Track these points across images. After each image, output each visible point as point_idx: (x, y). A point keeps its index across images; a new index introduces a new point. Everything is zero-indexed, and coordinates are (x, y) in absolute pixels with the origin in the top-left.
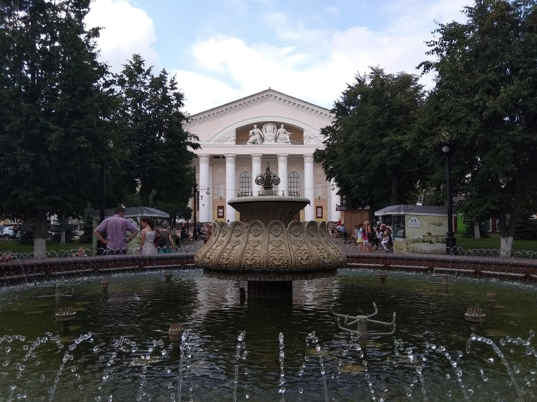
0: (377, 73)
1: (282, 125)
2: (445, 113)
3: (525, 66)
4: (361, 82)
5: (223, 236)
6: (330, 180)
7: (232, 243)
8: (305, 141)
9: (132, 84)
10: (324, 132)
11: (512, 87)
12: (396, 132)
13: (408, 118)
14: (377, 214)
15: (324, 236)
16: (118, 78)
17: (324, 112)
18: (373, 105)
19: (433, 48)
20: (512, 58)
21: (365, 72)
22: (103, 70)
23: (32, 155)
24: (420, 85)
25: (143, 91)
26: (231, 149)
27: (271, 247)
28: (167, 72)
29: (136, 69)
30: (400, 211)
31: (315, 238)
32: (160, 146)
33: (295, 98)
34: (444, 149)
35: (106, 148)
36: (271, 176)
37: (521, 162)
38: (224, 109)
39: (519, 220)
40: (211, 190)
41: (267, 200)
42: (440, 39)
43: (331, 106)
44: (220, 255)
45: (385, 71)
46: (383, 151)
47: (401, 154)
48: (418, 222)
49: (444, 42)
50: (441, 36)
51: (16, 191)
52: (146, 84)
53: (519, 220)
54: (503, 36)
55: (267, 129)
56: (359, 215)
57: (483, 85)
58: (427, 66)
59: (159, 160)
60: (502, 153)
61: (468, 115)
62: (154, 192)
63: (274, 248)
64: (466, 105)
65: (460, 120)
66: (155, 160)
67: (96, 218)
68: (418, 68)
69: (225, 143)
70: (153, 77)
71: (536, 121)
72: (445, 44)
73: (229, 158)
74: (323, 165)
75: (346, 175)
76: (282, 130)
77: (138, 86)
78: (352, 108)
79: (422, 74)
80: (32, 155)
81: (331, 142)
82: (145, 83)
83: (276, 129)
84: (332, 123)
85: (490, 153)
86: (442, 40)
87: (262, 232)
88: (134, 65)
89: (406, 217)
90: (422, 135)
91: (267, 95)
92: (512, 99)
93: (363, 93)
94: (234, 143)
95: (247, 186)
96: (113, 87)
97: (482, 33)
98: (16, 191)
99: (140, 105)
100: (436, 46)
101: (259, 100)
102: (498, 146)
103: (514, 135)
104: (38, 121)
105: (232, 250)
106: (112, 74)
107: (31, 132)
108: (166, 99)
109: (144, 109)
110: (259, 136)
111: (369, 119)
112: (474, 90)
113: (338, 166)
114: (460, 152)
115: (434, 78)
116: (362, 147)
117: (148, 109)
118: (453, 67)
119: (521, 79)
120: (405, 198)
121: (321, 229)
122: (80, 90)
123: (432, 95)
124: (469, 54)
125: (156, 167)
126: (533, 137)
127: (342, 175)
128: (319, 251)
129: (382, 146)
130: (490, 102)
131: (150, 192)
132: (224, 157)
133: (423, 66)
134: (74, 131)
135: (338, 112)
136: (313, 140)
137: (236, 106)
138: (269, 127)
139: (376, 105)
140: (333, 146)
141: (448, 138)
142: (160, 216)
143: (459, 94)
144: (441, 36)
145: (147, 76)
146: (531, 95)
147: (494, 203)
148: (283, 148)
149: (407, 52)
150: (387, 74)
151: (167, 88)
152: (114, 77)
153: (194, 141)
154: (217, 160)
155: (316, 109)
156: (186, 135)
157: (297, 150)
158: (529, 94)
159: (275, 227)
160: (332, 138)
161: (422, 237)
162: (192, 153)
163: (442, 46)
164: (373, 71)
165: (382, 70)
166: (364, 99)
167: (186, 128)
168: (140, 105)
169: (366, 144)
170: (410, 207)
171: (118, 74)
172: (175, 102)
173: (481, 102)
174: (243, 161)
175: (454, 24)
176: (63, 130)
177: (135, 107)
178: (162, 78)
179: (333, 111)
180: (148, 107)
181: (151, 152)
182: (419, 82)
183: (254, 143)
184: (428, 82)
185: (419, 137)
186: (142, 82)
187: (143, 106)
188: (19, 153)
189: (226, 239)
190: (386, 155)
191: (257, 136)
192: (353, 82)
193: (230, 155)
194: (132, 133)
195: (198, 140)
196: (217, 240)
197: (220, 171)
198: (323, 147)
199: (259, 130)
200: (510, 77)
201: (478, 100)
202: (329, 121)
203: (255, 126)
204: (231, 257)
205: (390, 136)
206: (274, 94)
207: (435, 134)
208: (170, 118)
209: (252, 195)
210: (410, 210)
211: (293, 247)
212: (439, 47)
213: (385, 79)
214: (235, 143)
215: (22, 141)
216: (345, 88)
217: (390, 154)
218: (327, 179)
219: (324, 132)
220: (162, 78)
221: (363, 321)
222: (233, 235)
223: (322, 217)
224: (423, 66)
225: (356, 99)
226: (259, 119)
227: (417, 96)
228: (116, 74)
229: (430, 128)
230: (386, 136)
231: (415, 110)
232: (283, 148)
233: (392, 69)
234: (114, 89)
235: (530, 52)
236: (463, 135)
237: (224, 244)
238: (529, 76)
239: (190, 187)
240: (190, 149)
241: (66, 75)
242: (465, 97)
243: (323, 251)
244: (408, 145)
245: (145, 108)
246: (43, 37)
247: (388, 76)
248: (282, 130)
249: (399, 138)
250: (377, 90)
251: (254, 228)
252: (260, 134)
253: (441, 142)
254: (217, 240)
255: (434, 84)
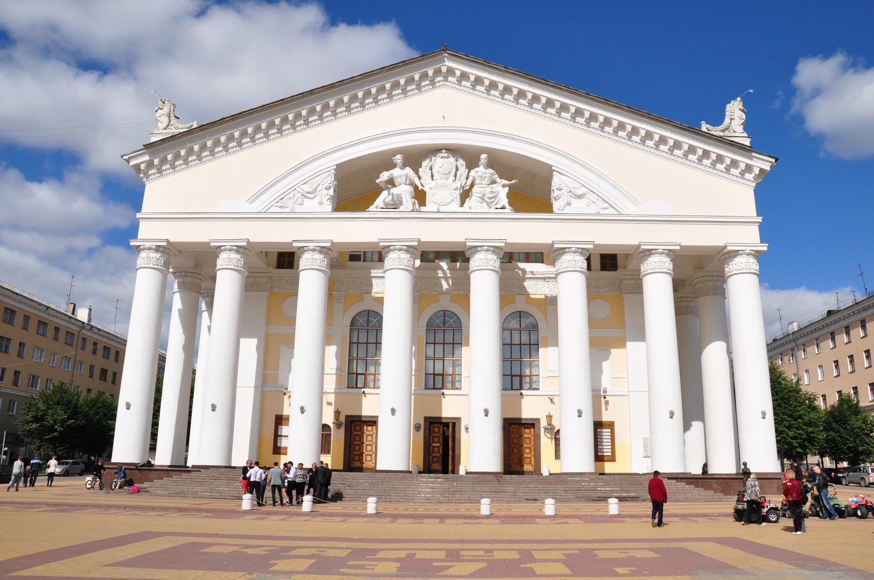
1: (484, 156)
8: (556, 206)
26: (320, 228)
76: (481, 172)
83: (463, 170)
94: (328, 207)
95: (516, 349)
110: (410, 189)
138: (442, 163)
148: (489, 223)
157: (529, 231)
174: (353, 264)
191: (404, 191)
199: (408, 170)
223: (612, 459)
232: (489, 223)
248: (481, 172)
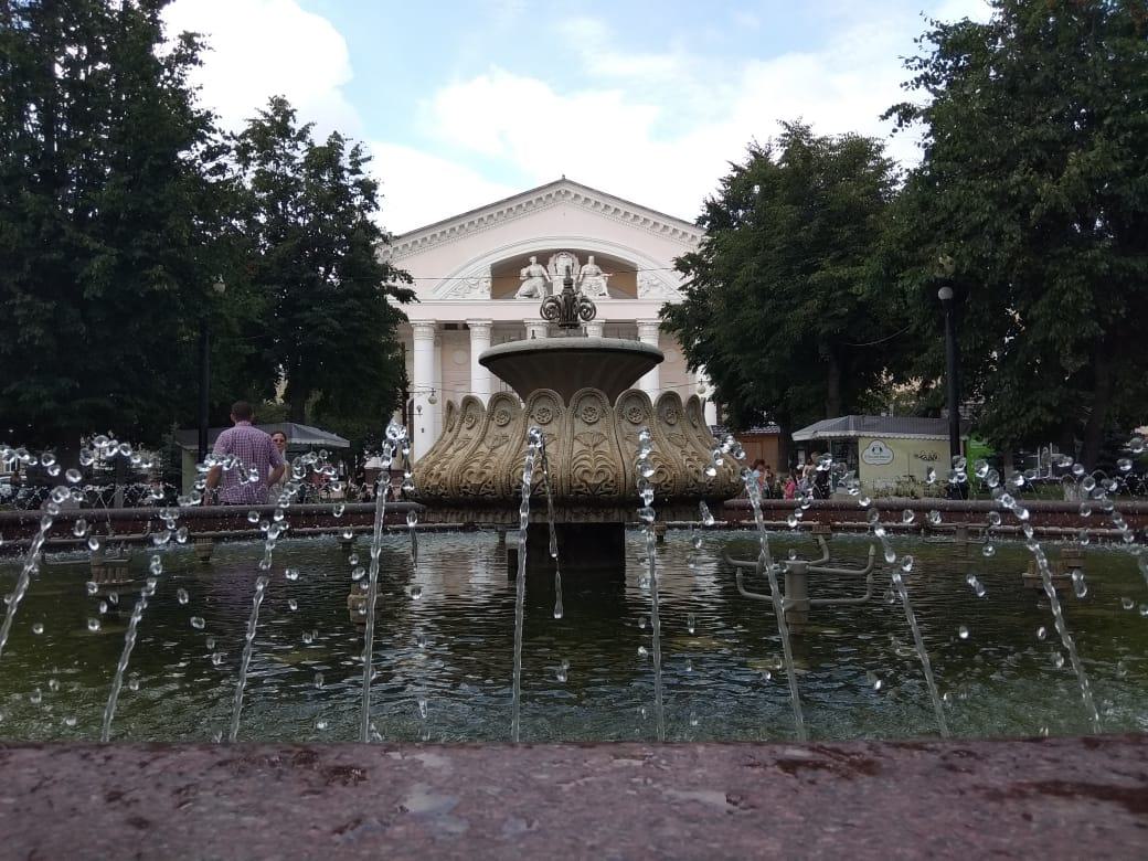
0: (796, 138)
1: (591, 258)
2: (945, 215)
3: (1117, 108)
4: (760, 158)
5: (469, 429)
6: (695, 371)
7: (489, 442)
8: (640, 292)
9: (264, 161)
10: (682, 265)
11: (1091, 155)
12: (836, 262)
13: (863, 231)
14: (798, 436)
15: (695, 427)
16: (234, 141)
17: (682, 228)
18: (786, 204)
19: (920, 73)
20: (1089, 92)
21: (769, 136)
22: (200, 125)
23: (49, 306)
24: (889, 159)
25: (290, 175)
26: (480, 308)
27: (578, 447)
28: (343, 137)
29: (273, 130)
30: (847, 429)
31: (678, 430)
32: (330, 295)
33: (619, 199)
34: (943, 293)
35: (210, 294)
36: (575, 299)
37: (1110, 318)
38: (465, 222)
39: (1101, 451)
40: (438, 395)
41: (569, 346)
42: (934, 53)
43: (693, 210)
44: (464, 467)
45: (812, 131)
46: (809, 303)
47: (849, 308)
48: (886, 452)
49: (942, 61)
50: (937, 47)
51: (13, 387)
52: (296, 161)
53: (1101, 451)
54: (1069, 46)
55: (559, 266)
56: (758, 445)
57: (1026, 151)
58: (906, 113)
59: (327, 324)
60: (1069, 297)
61: (994, 216)
62: (316, 396)
63: (585, 448)
64: (991, 195)
65: (977, 230)
66: (317, 325)
67: (188, 448)
68: (884, 118)
69: (468, 297)
70: (311, 144)
71: (1139, 231)
72: (943, 67)
73: (477, 329)
74: (680, 335)
75: (730, 356)
76: (590, 267)
77: (278, 165)
78: (741, 212)
79: (895, 131)
80: (49, 306)
81: (696, 288)
82: (294, 158)
84: (700, 246)
85: (1044, 300)
86: (938, 58)
87: (558, 414)
88: (271, 119)
89: (861, 442)
90: (895, 264)
91: (559, 191)
92: (1090, 180)
93: (765, 180)
96: (222, 159)
97: (1025, 41)
98: (13, 387)
99: (285, 207)
100: (925, 70)
101: (540, 204)
102: (1061, 282)
103: (1095, 259)
104: (61, 232)
105: (490, 455)
106: (223, 133)
107: (47, 257)
108: (341, 193)
109: (291, 214)
110: (541, 280)
111: (779, 233)
112: (1006, 164)
113: (712, 338)
114: (973, 300)
115: (920, 139)
116: (763, 293)
117: (300, 214)
118: (964, 113)
119: (1110, 137)
120: (856, 398)
121: (690, 412)
122: (151, 165)
123: (915, 177)
124: (998, 85)
125: (320, 340)
126: (1133, 264)
127: (720, 356)
128: (685, 458)
129: (807, 291)
130: (1046, 186)
131: (308, 396)
132: (466, 327)
133: (895, 116)
134: (139, 254)
135: (713, 222)
136: (659, 289)
137: (492, 216)
139: (795, 203)
140: (703, 295)
141: (950, 269)
142: (329, 443)
143: (974, 173)
144: (937, 47)
145: (300, 144)
146: (1133, 172)
147: (1051, 410)
149: (863, 89)
150: (817, 137)
151: (342, 169)
152: (226, 138)
153: (400, 284)
154: (451, 333)
155: (663, 222)
156: (385, 271)
158: (1125, 170)
159: (587, 404)
160: (700, 279)
161: (894, 485)
162: (397, 312)
163: (937, 70)
164: (787, 131)
165: (808, 127)
166: (765, 193)
167: (382, 255)
168: (285, 207)
169: (772, 287)
170: (869, 419)
171: (235, 133)
172: (357, 201)
173: (1023, 188)
175: (966, 23)
176: (115, 251)
177: (272, 209)
178: (336, 142)
179: (701, 220)
180: (302, 211)
181: (309, 308)
182: (884, 155)
183: (530, 296)
184: (906, 151)
185: (887, 270)
186: (287, 155)
187: (290, 209)
188: (18, 302)
189: (475, 434)
190: (816, 311)
192: (743, 160)
193: (479, 323)
194: (268, 264)
195: (410, 282)
196: (456, 436)
197: (459, 356)
198: (679, 298)
200: (1082, 135)
201: (1018, 184)
202: (692, 244)
203: (533, 259)
204: (487, 471)
205: (824, 269)
206: (573, 191)
207: (922, 263)
208: (349, 234)
209: (534, 338)
210: (869, 428)
211: (629, 447)
212: (930, 73)
213: (814, 148)
214: (489, 297)
215: (25, 277)
216: (728, 172)
217: (825, 309)
218: (689, 368)
219: (682, 265)
220: (336, 142)
221: (797, 571)
222: (493, 425)
224: (895, 116)
225: (751, 194)
226: (540, 244)
227: (883, 185)
228: (231, 133)
229: (913, 245)
230: (815, 269)
231: (878, 212)
233: (831, 125)
234: (226, 165)
235: (1128, 79)
236: (982, 262)
237: (473, 444)
238: (1125, 130)
239: (391, 392)
240: (392, 300)
241: (121, 133)
242: (988, 178)
243: (695, 458)
244: (861, 290)
245: (294, 213)
246: (72, 51)
247: (819, 141)
248: (590, 267)
249: (843, 272)
250: (796, 172)
251: (538, 407)
252: (543, 276)
253: (936, 279)
254: (456, 436)
255: (920, 154)
